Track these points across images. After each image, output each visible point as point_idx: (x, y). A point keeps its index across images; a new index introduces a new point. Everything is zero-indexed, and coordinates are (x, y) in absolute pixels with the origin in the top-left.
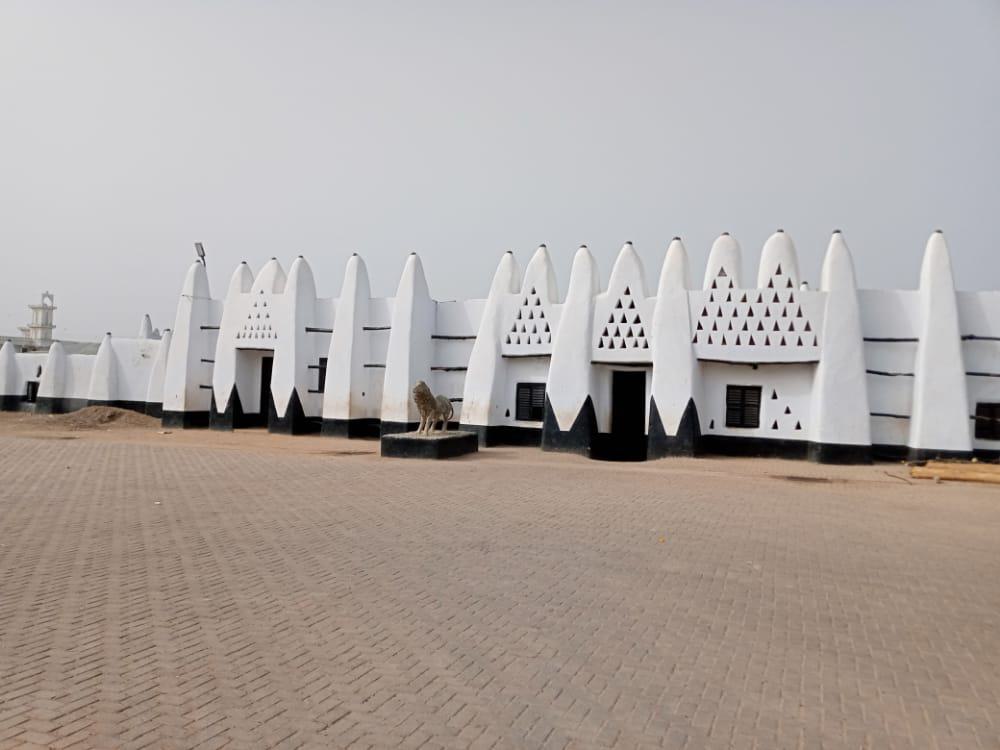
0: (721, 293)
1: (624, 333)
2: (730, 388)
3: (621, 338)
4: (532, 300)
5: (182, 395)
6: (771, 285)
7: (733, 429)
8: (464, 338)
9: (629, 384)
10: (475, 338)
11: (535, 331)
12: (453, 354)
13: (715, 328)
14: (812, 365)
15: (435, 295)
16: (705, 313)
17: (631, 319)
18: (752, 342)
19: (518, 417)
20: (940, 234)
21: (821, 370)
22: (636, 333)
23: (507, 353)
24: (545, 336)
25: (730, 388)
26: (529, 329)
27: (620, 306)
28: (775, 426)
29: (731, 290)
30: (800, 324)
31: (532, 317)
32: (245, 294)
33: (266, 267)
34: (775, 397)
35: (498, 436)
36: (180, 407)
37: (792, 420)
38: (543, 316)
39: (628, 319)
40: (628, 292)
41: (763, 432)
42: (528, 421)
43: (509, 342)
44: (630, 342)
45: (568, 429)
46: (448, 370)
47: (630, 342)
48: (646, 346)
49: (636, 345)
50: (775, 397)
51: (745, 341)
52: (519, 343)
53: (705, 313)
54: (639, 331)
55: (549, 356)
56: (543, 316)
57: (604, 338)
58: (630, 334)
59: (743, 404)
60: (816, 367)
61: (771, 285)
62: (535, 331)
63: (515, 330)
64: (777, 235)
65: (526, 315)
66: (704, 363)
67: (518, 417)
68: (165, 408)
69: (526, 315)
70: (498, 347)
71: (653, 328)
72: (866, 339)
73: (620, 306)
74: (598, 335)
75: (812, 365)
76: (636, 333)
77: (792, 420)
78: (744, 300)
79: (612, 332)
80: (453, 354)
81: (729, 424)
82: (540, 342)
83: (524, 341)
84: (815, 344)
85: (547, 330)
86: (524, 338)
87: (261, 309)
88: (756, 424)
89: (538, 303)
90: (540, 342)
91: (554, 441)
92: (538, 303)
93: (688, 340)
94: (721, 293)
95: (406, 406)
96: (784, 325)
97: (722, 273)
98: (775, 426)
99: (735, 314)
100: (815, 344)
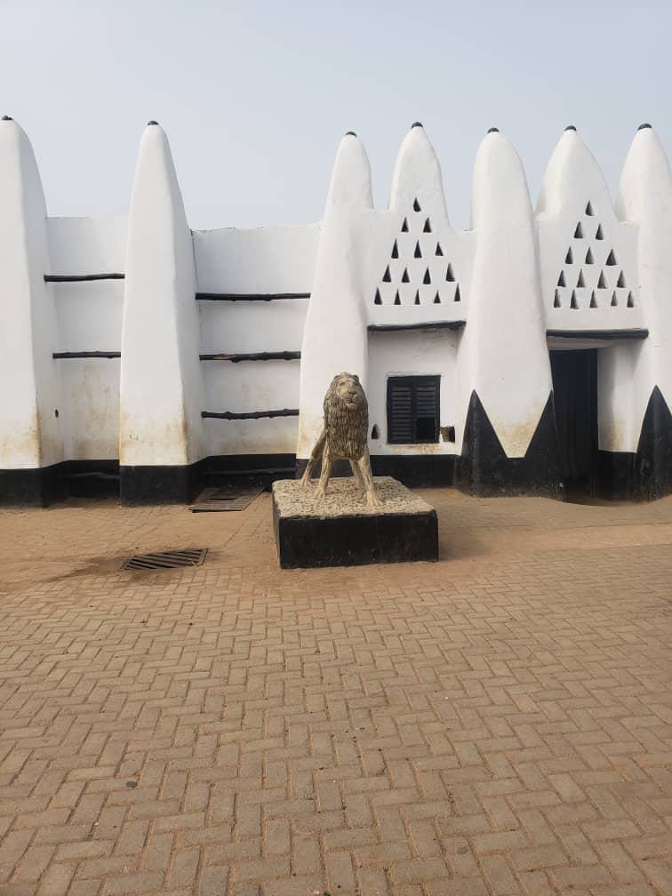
1: (416, 277)
5: (177, 433)
8: (268, 298)
10: (308, 296)
11: (427, 280)
12: (254, 330)
14: (456, 328)
15: (195, 224)
17: (600, 258)
19: (392, 440)
21: (469, 333)
22: (611, 282)
23: (379, 322)
24: (447, 291)
26: (416, 277)
30: (611, 275)
31: (418, 254)
33: (562, 141)
36: (173, 455)
38: (439, 252)
43: (378, 301)
44: (603, 297)
45: (521, 454)
46: (237, 359)
47: (427, 293)
52: (397, 302)
56: (439, 252)
60: (463, 330)
62: (427, 280)
63: (387, 278)
65: (406, 251)
66: (373, 330)
67: (392, 440)
68: (121, 464)
69: (406, 251)
70: (363, 312)
72: (199, 296)
74: (551, 285)
75: (456, 328)
76: (611, 282)
79: (571, 281)
80: (254, 330)
82: (437, 300)
84: (417, 302)
85: (450, 278)
90: (437, 300)
91: (498, 476)
92: (427, 229)
95: (181, 429)
100: (417, 302)
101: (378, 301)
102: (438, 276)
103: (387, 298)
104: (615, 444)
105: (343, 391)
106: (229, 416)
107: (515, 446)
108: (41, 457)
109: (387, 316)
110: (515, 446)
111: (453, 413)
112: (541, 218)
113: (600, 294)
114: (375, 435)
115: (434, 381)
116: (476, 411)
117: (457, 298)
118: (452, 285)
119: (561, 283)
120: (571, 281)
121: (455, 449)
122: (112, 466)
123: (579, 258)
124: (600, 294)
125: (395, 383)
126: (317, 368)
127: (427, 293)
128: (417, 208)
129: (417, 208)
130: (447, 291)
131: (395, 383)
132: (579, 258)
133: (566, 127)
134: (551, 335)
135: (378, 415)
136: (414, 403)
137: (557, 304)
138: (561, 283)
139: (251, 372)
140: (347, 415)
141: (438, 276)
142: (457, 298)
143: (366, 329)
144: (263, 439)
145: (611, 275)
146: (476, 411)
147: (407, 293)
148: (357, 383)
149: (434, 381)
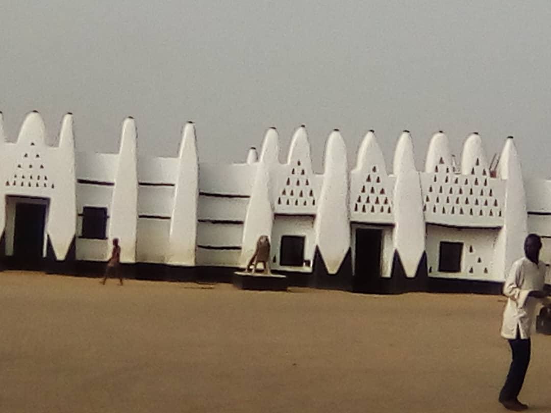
0: (442, 175)
1: (372, 201)
2: (442, 243)
3: (479, 206)
4: (298, 170)
6: (473, 172)
7: (444, 273)
9: (369, 238)
11: (301, 195)
12: (224, 210)
13: (438, 201)
14: (497, 230)
16: (431, 190)
18: (462, 212)
19: (282, 264)
20: (36, 114)
21: (503, 234)
22: (382, 201)
25: (442, 243)
27: (369, 179)
28: (471, 271)
29: (448, 174)
30: (382, 198)
32: (11, 144)
34: (471, 250)
35: (424, 282)
36: (189, 261)
37: (482, 266)
39: (375, 187)
40: (374, 170)
41: (464, 274)
42: (364, 265)
43: (279, 202)
48: (389, 211)
49: (382, 210)
50: (471, 250)
51: (457, 211)
52: (444, 212)
53: (431, 190)
54: (384, 199)
55: (313, 217)
56: (307, 184)
57: (358, 204)
58: (377, 202)
59: (451, 256)
61: (473, 172)
62: (301, 195)
63: (284, 193)
64: (439, 135)
69: (293, 182)
71: (396, 198)
72: (529, 213)
73: (369, 179)
74: (354, 201)
76: (382, 201)
77: (482, 266)
78: (456, 182)
81: (440, 270)
83: (292, 203)
84: (500, 215)
86: (292, 200)
87: (31, 159)
88: (457, 269)
89: (303, 173)
92: (303, 173)
93: (421, 208)
94: (442, 175)
96: (482, 200)
97: (441, 161)
98: (471, 271)
99: (451, 192)
101: (279, 202)
102: (306, 194)
103: (284, 201)
104: (384, 272)
105: (262, 241)
106: (209, 248)
107: (332, 269)
108: (136, 259)
109: (283, 209)
110: (332, 269)
111: (309, 255)
112: (353, 172)
113: (376, 206)
114: (275, 260)
115: (302, 239)
116: (397, 259)
117: (314, 203)
118: (312, 198)
119: (359, 200)
120: (364, 200)
121: (307, 269)
122: (164, 266)
123: (368, 190)
124: (376, 206)
125: (284, 238)
126: (252, 231)
127: (301, 201)
128: (299, 164)
129: (299, 164)
130: (310, 200)
131: (284, 238)
132: (368, 190)
133: (507, 136)
134: (352, 223)
135: (276, 251)
136: (293, 248)
137: (356, 209)
138: (359, 200)
139: (220, 228)
140: (263, 249)
141: (306, 194)
142: (314, 203)
143: (273, 215)
144: (224, 259)
145: (382, 198)
146: (397, 259)
147: (292, 200)
148: (267, 240)
149: (302, 239)
